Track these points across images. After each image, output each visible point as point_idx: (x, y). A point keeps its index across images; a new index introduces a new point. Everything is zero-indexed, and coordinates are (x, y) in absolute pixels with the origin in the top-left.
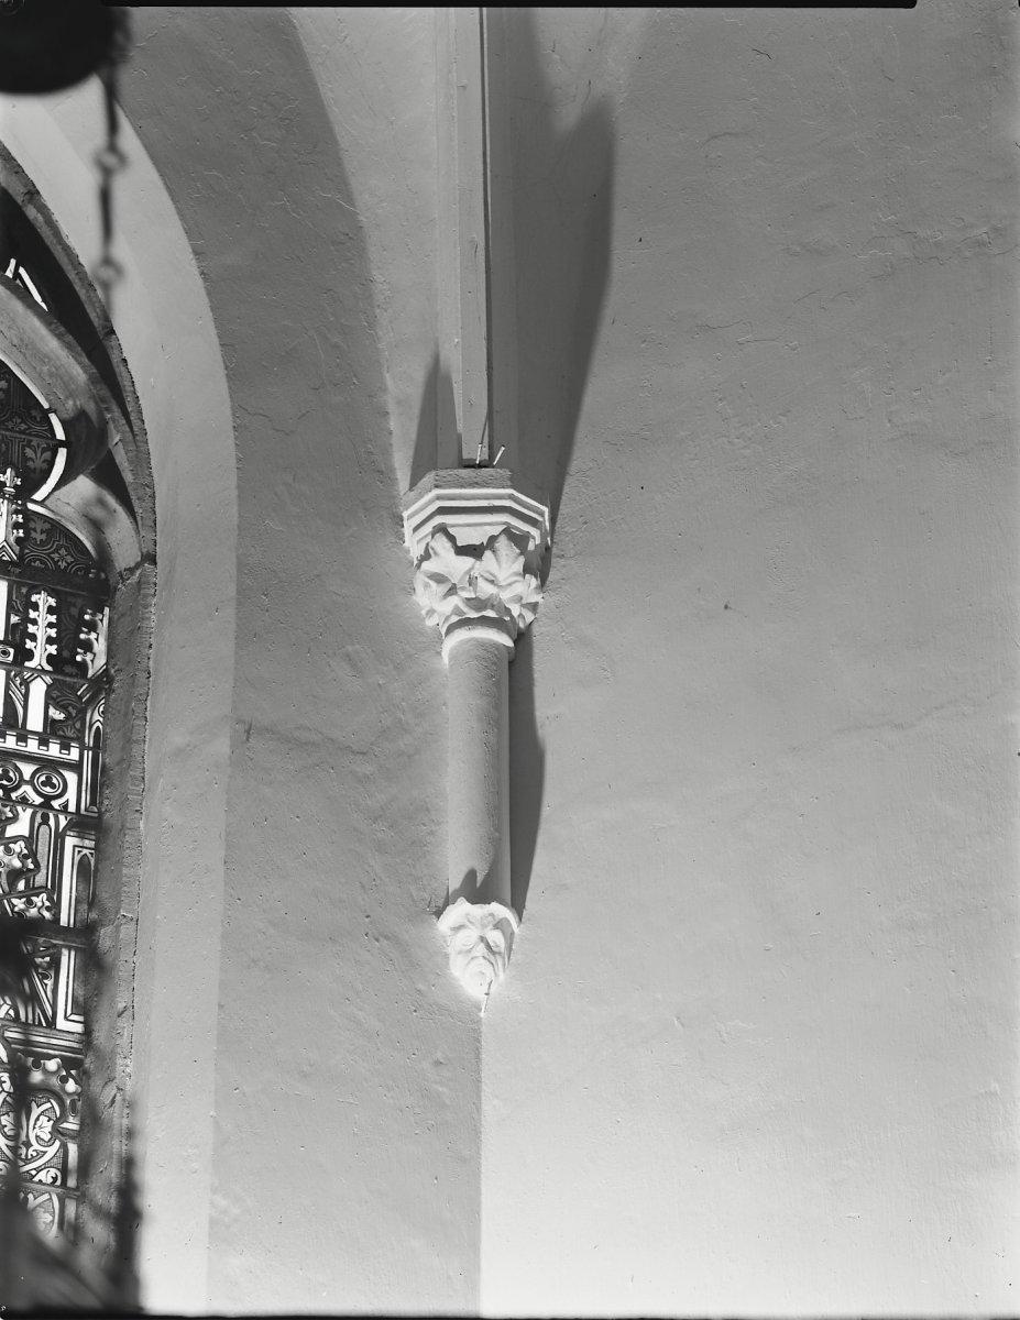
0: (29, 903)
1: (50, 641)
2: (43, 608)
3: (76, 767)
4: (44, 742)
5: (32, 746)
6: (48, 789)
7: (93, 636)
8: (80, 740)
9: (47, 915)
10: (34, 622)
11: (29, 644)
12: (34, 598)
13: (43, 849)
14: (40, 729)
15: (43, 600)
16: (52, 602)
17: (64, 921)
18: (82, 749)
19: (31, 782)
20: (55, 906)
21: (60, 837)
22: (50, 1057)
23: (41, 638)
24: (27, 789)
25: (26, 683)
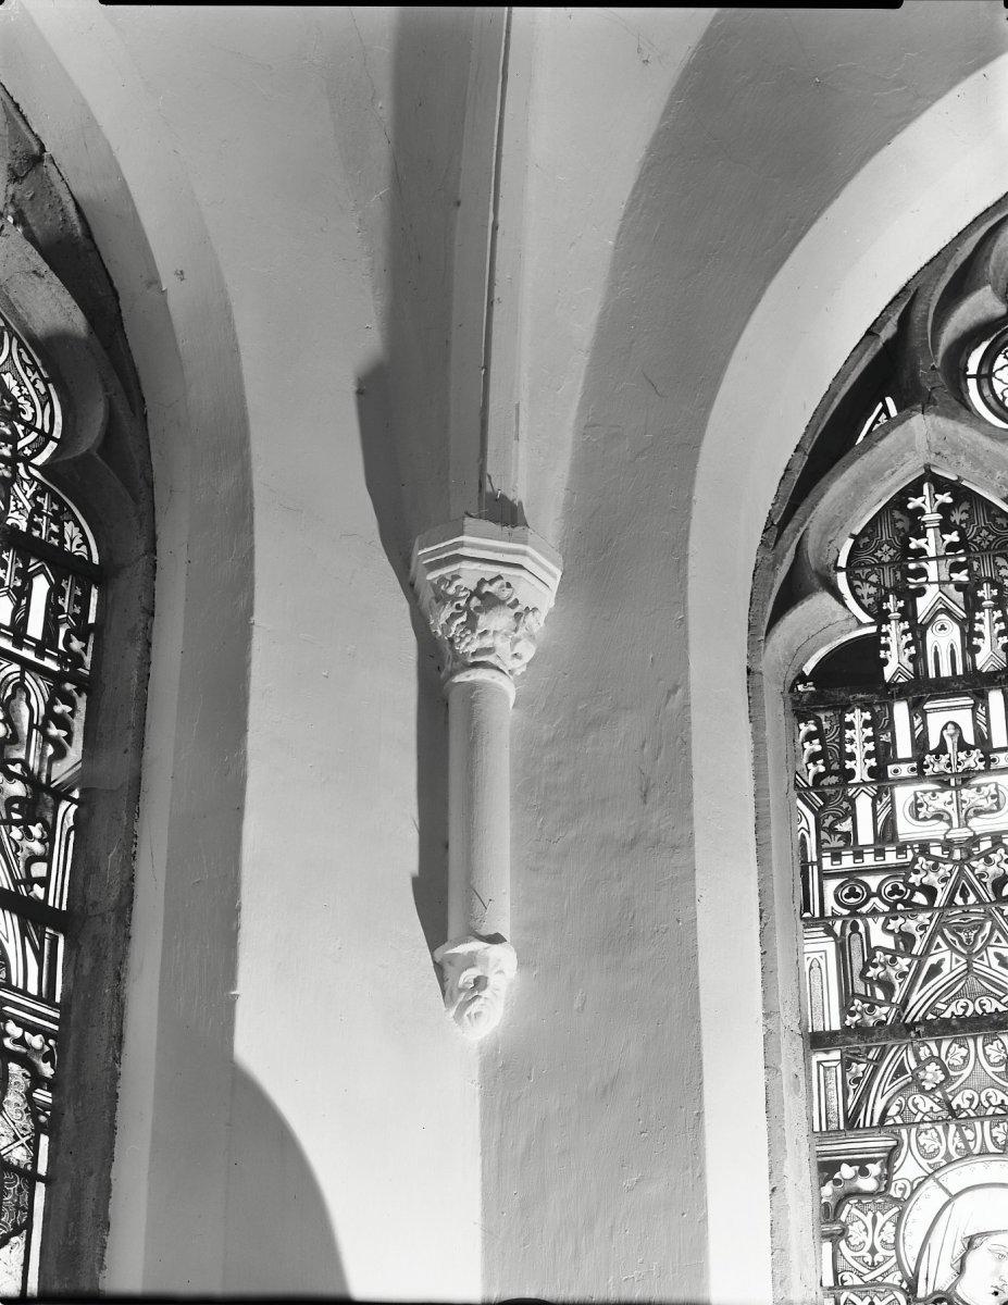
4: (880, 853)
5: (869, 860)
6: (852, 900)
10: (852, 741)
11: (849, 765)
12: (849, 718)
16: (867, 716)
17: (22, 886)
19: (878, 894)
23: (859, 755)
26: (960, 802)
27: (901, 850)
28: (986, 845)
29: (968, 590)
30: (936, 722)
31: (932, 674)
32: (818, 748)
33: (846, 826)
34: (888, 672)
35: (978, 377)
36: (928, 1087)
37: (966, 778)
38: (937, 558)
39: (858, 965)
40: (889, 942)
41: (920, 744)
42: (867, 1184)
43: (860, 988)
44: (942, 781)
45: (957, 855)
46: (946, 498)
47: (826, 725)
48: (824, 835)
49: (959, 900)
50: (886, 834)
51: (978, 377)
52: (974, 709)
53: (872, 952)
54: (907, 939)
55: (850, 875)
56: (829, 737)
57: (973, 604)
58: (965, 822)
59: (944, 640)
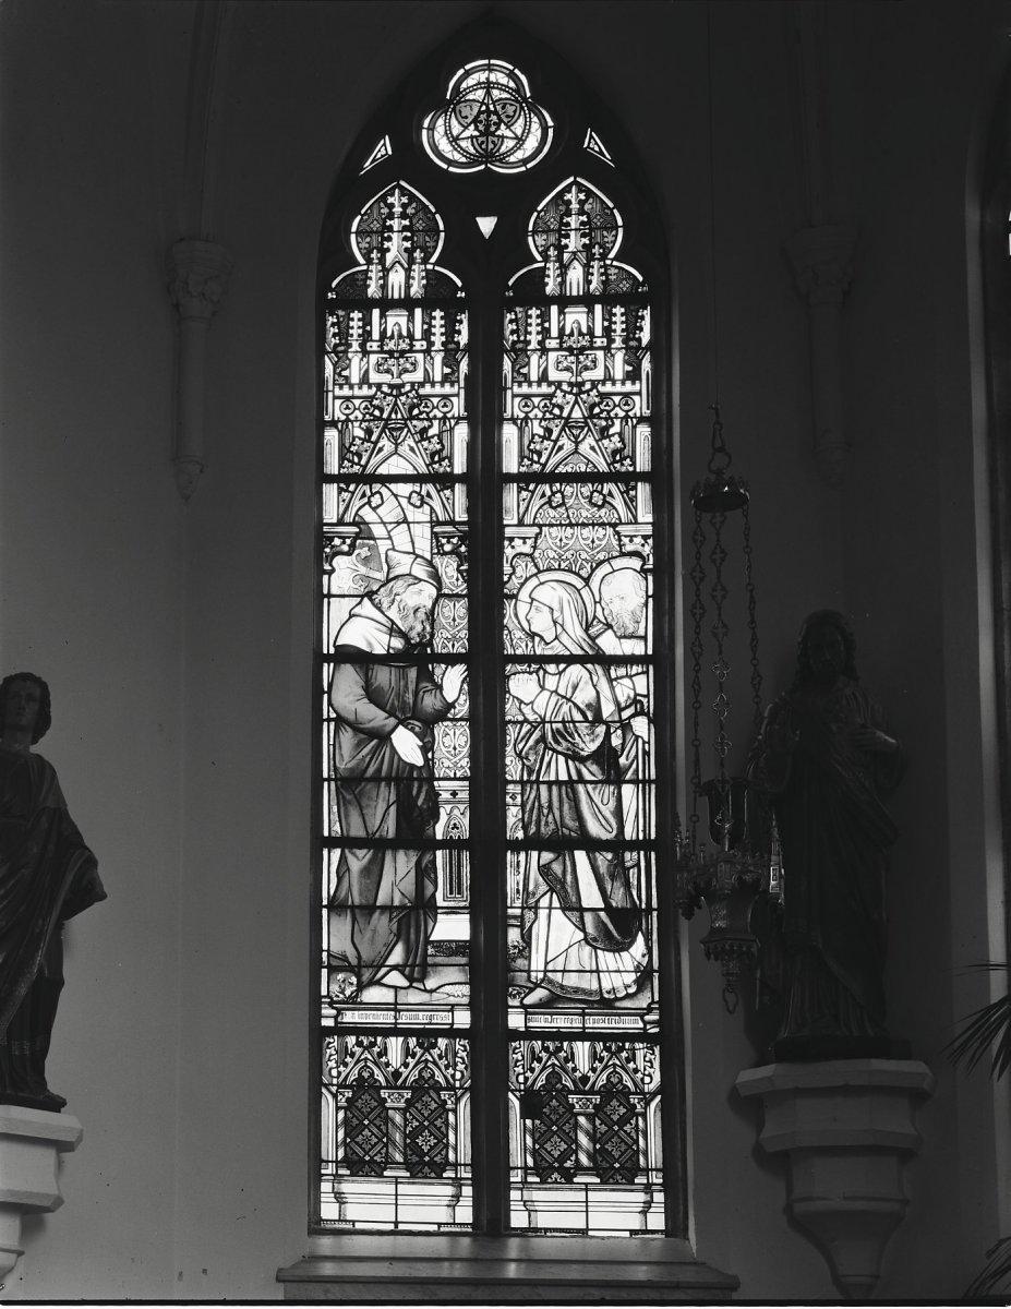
0: (622, 465)
2: (438, 318)
9: (448, 469)
11: (529, 337)
25: (613, 355)
26: (578, 362)
27: (370, 387)
28: (408, 388)
29: (409, 251)
30: (391, 321)
31: (390, 297)
32: (515, 327)
33: (524, 371)
34: (548, 290)
35: (428, 129)
36: (554, 505)
37: (582, 350)
38: (576, 230)
39: (526, 442)
40: (361, 434)
41: (383, 334)
42: (345, 548)
43: (527, 452)
44: (570, 350)
45: (394, 393)
46: (405, 200)
47: (519, 316)
48: (337, 377)
49: (393, 416)
50: (543, 378)
51: (428, 129)
52: (588, 313)
53: (533, 436)
54: (549, 431)
55: (348, 399)
56: (343, 325)
57: (411, 261)
58: (579, 373)
59: (576, 274)
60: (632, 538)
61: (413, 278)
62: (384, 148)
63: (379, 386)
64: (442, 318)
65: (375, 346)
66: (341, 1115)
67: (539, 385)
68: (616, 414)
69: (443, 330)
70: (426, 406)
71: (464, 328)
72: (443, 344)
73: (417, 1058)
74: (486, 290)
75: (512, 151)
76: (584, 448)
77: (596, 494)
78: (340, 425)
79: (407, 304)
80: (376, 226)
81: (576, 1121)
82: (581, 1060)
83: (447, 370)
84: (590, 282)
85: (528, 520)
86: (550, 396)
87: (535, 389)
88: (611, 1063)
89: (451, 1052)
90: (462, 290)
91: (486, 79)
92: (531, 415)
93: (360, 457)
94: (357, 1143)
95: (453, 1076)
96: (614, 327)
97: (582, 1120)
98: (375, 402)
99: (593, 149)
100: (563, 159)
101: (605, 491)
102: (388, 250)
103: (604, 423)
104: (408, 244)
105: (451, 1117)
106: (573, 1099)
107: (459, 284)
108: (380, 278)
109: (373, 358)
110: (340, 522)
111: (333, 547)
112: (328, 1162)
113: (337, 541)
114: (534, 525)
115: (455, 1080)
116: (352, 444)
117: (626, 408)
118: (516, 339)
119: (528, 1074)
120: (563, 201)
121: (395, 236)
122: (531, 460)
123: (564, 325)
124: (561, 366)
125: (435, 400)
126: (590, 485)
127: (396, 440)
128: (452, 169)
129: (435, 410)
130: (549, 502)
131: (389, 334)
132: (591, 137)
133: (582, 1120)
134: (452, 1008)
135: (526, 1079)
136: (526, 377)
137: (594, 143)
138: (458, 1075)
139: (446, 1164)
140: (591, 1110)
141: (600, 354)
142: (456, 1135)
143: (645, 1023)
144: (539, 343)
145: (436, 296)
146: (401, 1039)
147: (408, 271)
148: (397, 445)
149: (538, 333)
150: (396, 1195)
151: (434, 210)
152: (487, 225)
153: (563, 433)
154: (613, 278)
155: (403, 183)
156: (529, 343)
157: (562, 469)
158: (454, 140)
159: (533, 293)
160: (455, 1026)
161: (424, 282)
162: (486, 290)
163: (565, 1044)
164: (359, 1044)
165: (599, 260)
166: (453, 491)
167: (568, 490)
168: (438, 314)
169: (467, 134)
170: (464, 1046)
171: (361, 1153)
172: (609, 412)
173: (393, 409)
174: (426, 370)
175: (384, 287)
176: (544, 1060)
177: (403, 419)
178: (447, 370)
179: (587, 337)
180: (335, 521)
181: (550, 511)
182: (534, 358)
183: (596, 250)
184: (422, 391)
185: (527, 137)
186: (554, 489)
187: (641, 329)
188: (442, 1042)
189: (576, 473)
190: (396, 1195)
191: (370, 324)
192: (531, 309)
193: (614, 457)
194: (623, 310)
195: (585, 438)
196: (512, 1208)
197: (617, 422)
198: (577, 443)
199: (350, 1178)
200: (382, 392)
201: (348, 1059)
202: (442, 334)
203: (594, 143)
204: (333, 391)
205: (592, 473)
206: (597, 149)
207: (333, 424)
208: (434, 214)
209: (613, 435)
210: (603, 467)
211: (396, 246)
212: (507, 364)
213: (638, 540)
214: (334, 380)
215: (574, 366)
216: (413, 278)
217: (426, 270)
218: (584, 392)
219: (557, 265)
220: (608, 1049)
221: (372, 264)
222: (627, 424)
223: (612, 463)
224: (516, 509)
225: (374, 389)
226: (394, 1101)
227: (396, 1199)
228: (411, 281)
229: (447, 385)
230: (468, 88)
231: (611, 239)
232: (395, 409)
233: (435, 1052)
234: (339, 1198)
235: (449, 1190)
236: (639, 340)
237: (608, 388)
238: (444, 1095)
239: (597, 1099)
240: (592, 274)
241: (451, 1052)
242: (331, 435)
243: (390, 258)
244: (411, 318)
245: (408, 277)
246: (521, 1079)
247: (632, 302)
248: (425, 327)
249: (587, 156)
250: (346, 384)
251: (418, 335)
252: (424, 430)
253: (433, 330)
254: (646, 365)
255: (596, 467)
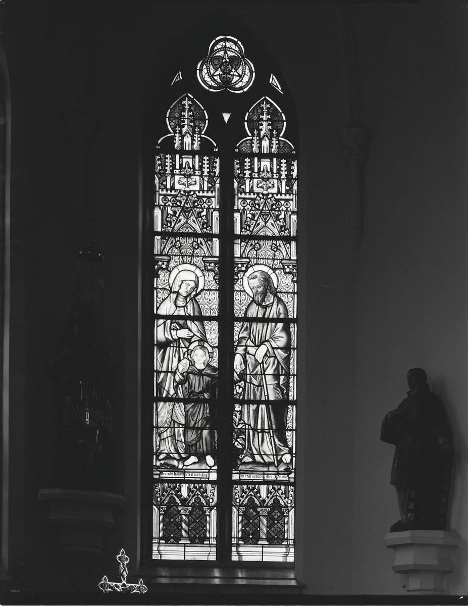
0: (207, 230)
1: (170, 166)
2: (283, 163)
3: (292, 200)
5: (205, 194)
7: (294, 167)
8: (293, 193)
9: (288, 234)
13: (287, 220)
14: (206, 189)
15: (206, 158)
18: (293, 195)
20: (290, 233)
21: (290, 216)
22: (211, 263)
24: (283, 207)
25: (281, 182)
28: (270, 196)
29: (193, 128)
30: (263, 164)
31: (184, 149)
37: (189, 176)
41: (259, 169)
44: (185, 175)
46: (268, 106)
49: (264, 209)
50: (251, 191)
56: (163, 161)
57: (194, 132)
60: (288, 266)
61: (195, 140)
62: (180, 76)
63: (258, 194)
64: (285, 163)
65: (177, 172)
66: (161, 517)
67: (250, 194)
68: (204, 206)
69: (286, 169)
70: (201, 202)
71: (295, 168)
72: (208, 172)
73: (272, 494)
74: (226, 151)
75: (236, 82)
76: (269, 224)
77: (195, 243)
78: (241, 211)
79: (192, 153)
80: (177, 115)
81: (181, 518)
82: (263, 493)
83: (288, 188)
84: (272, 148)
85: (164, 253)
86: (254, 200)
87: (248, 196)
88: (275, 495)
89: (286, 492)
90: (294, 150)
91: (228, 47)
92: (246, 208)
93: (250, 227)
94: (272, 531)
95: (287, 502)
96: (204, 166)
97: (184, 517)
98: (256, 202)
99: (273, 84)
100: (260, 87)
101: (199, 242)
102: (261, 130)
103: (277, 213)
104: (270, 127)
105: (208, 518)
106: (259, 509)
107: (215, 145)
108: (258, 143)
109: (255, 181)
110: (241, 257)
111: (158, 265)
112: (234, 538)
113: (160, 263)
114: (247, 258)
115: (288, 504)
116: (167, 217)
117: (287, 206)
118: (239, 172)
119: (241, 498)
120: (260, 108)
121: (264, 123)
122: (246, 229)
123: (182, 163)
124: (259, 186)
125: (205, 199)
126: (192, 238)
127: (265, 220)
128: (211, 90)
129: (248, 206)
130: (175, 246)
131: (262, 170)
132: (273, 78)
133: (184, 517)
134: (209, 471)
135: (240, 500)
136: (244, 190)
137: (274, 81)
138: (289, 502)
139: (283, 540)
140: (188, 513)
141: (276, 181)
142: (210, 526)
143: (289, 478)
144: (171, 171)
145: (205, 150)
146: (266, 486)
147: (192, 137)
148: (265, 222)
149: (170, 166)
150: (263, 552)
151: (281, 111)
152: (226, 117)
153: (260, 217)
154: (282, 146)
155: (267, 98)
156: (166, 170)
157: (183, 230)
158: (212, 77)
159: (169, 147)
160: (210, 479)
161: (200, 143)
162: (226, 151)
163: (203, 485)
164: (169, 487)
165: (198, 134)
166: (290, 245)
167: (262, 243)
168: (283, 161)
169: (217, 73)
170: (292, 489)
171: (273, 535)
172: (279, 208)
173: (264, 205)
174: (278, 187)
175: (260, 148)
176: (273, 493)
177: (191, 207)
178: (288, 188)
179: (192, 170)
180: (239, 256)
181: (175, 249)
182: (247, 181)
183: (274, 132)
184: (276, 197)
185: (244, 76)
186: (177, 239)
187: (293, 170)
188: (283, 488)
189: (187, 233)
190: (263, 552)
191: (254, 164)
192: (217, 158)
193: (203, 225)
194: (208, 158)
195: (191, 216)
196: (232, 554)
197: (283, 213)
198: (187, 219)
199: (165, 545)
200: (259, 197)
201: (165, 493)
202: (285, 171)
203: (274, 81)
204: (159, 191)
205: (194, 233)
206: (275, 84)
207: (238, 211)
208: (203, 110)
209: (281, 219)
210: (277, 234)
211: (265, 128)
212: (157, 181)
213: (212, 265)
214: (159, 186)
215: (186, 183)
216: (195, 140)
217: (200, 137)
218: (190, 196)
219: (258, 138)
220: (274, 489)
221: (196, 134)
222: (287, 214)
223: (203, 229)
224: (239, 249)
225: (256, 195)
226: (263, 511)
227: (185, 553)
228: (253, 145)
229: (210, 193)
230: (218, 49)
231: (202, 125)
232: (186, 202)
233: (280, 492)
234: (238, 552)
235: (284, 550)
236: (215, 173)
237: (279, 197)
238: (283, 510)
239: (269, 509)
240: (273, 144)
241: (286, 492)
242: (237, 216)
243: (262, 133)
244: (272, 161)
245: (193, 140)
246: (238, 500)
247: (289, 158)
248: (278, 167)
249: (270, 85)
250: (243, 192)
251: (197, 168)
252: (199, 213)
253: (282, 169)
254: (295, 187)
255: (274, 234)
